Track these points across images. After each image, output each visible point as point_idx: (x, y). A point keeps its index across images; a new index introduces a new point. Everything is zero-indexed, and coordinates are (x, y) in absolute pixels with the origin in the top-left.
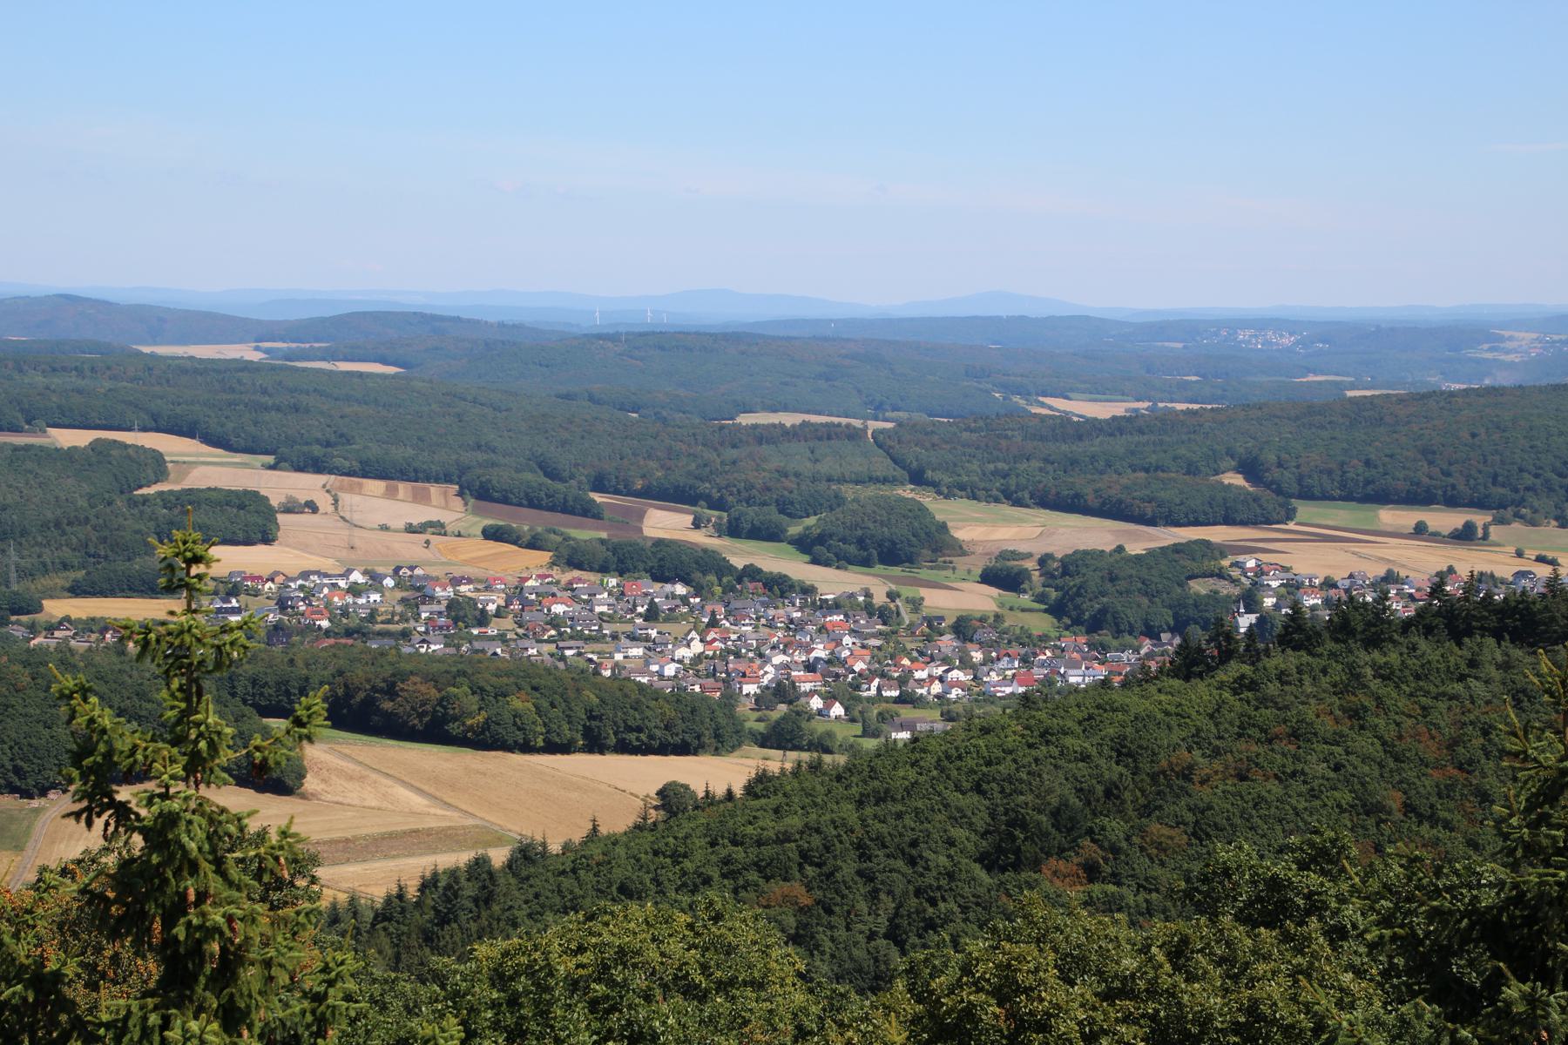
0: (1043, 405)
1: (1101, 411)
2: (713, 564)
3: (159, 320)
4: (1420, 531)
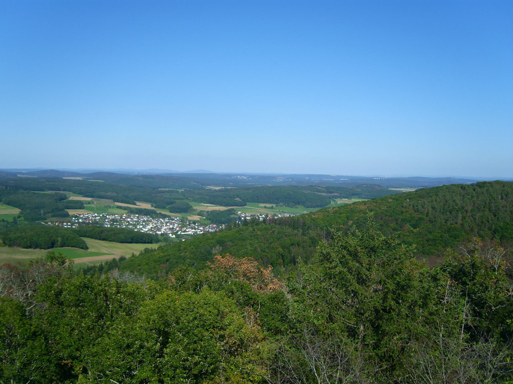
0: (207, 187)
1: (217, 188)
2: (154, 212)
3: (63, 173)
4: (265, 207)
